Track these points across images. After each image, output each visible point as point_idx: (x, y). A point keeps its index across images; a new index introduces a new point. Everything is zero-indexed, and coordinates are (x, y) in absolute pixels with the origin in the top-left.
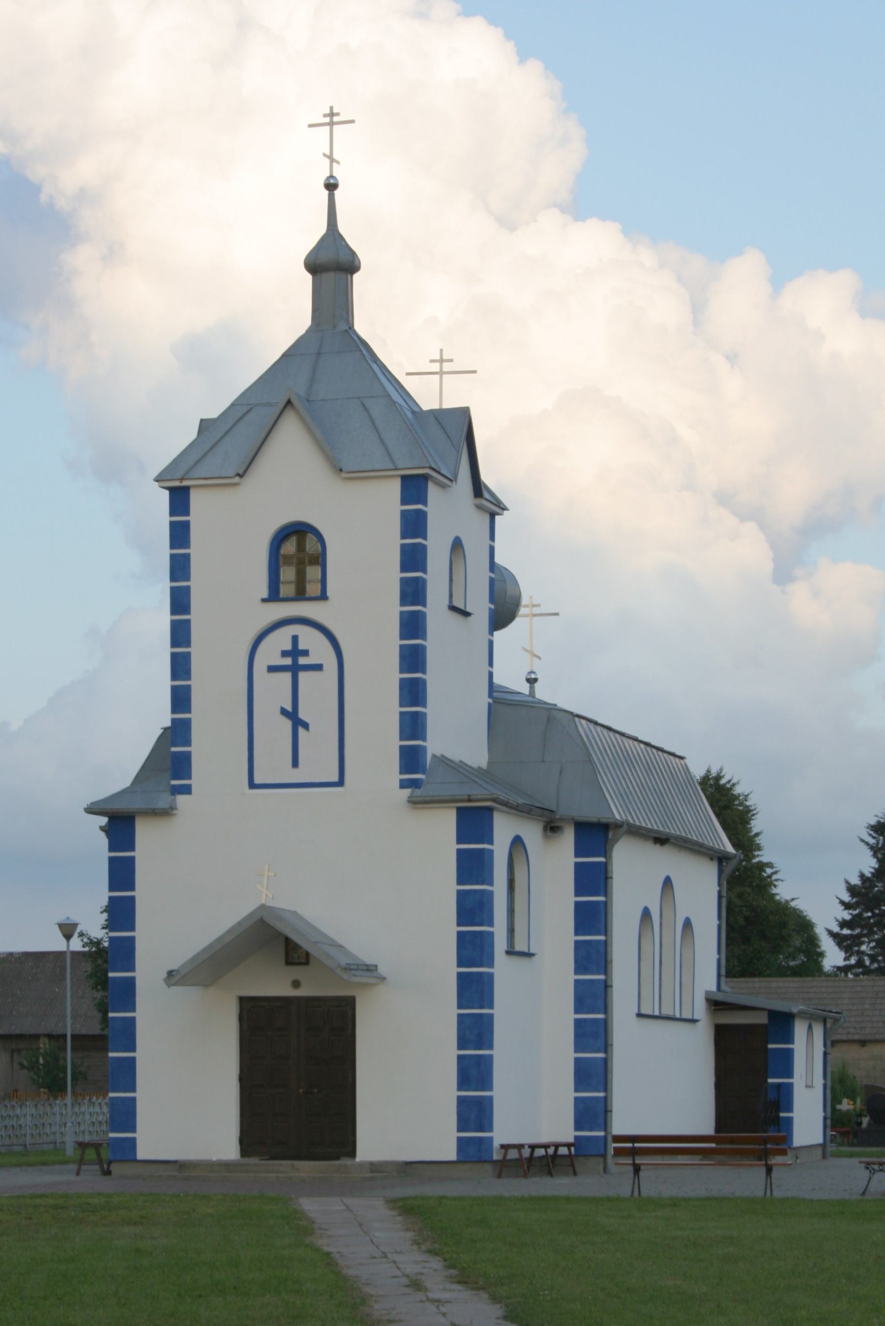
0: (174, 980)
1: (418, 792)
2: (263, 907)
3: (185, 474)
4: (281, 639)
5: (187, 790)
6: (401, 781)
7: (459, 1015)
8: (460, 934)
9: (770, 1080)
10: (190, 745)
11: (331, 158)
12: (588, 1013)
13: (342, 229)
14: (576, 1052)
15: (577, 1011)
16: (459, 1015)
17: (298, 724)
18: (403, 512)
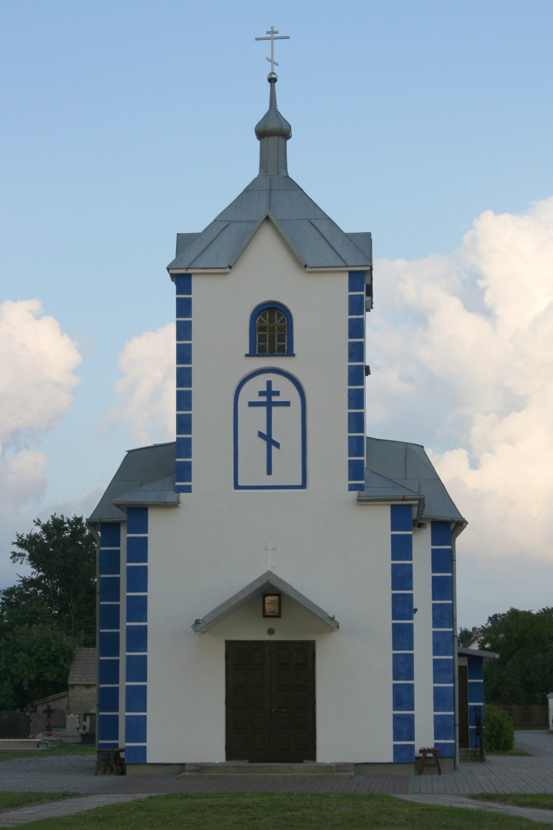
0: (199, 627)
1: (363, 493)
2: (269, 573)
3: (190, 265)
4: (259, 384)
5: (188, 489)
6: (349, 485)
7: (394, 655)
8: (394, 595)
9: (470, 704)
10: (190, 457)
11: (271, 61)
12: (443, 655)
13: (280, 108)
14: (434, 682)
15: (435, 654)
16: (394, 655)
17: (271, 443)
18: (350, 297)
